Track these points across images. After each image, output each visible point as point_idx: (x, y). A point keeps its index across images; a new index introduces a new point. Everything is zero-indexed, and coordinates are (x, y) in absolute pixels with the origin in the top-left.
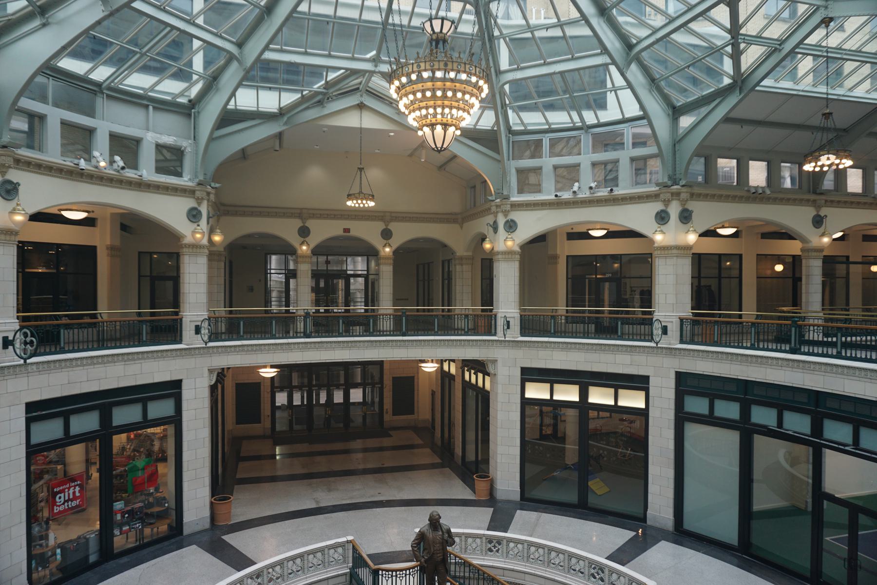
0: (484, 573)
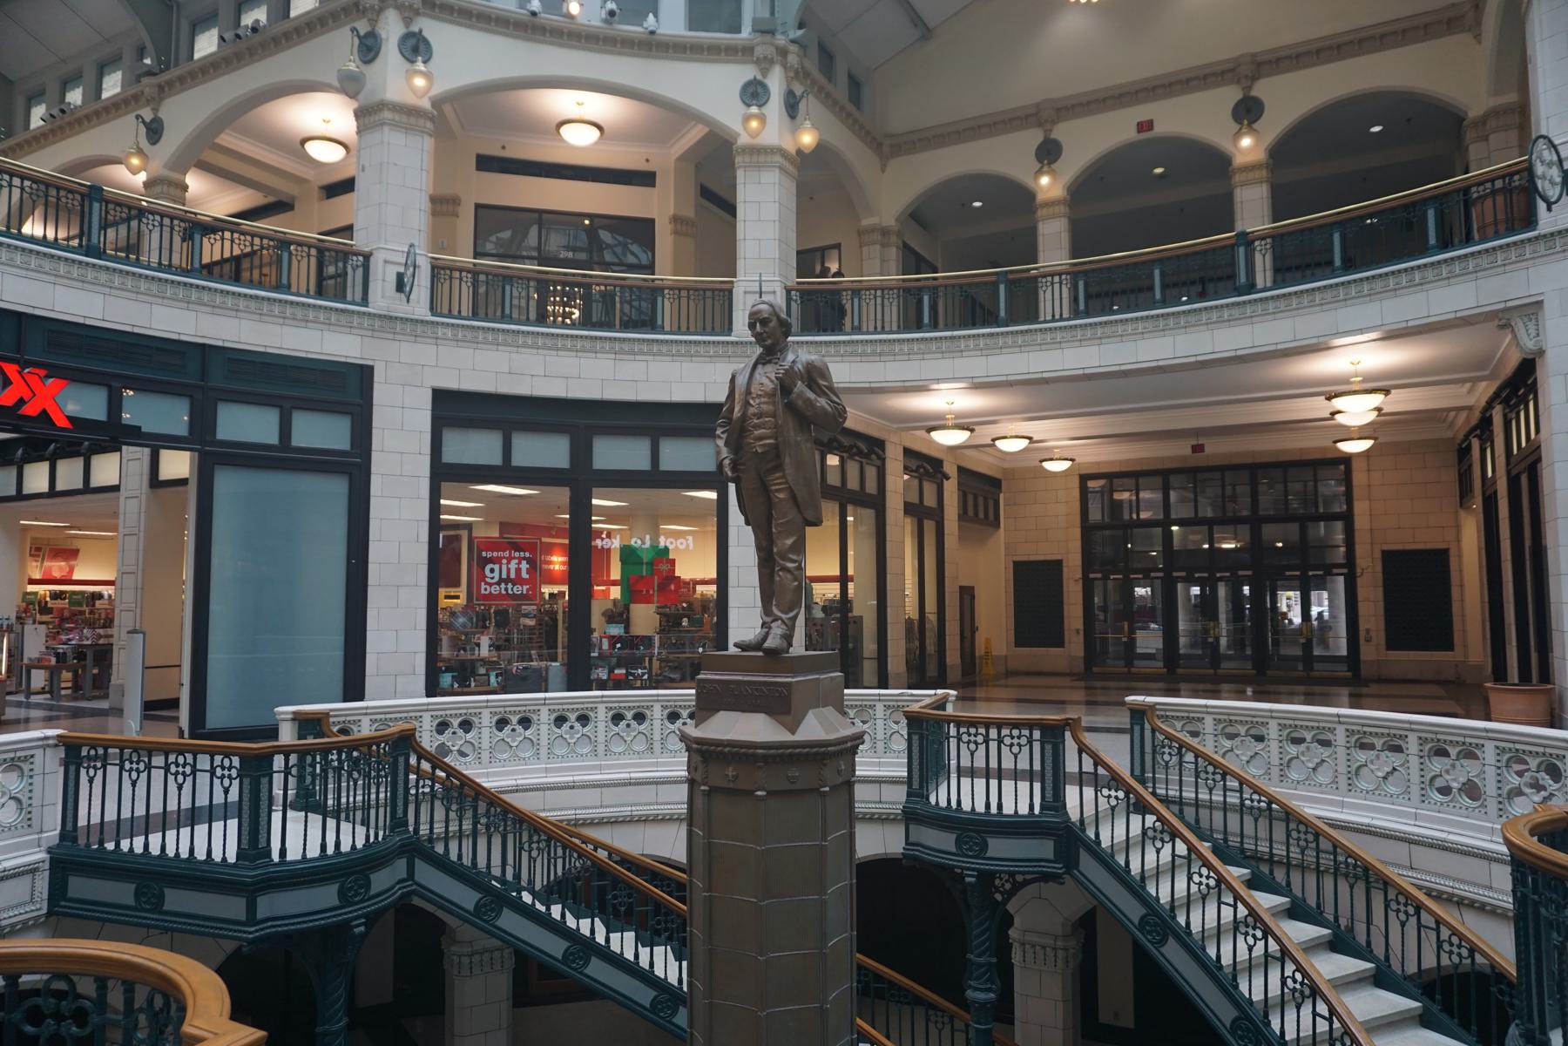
0: (1336, 845)
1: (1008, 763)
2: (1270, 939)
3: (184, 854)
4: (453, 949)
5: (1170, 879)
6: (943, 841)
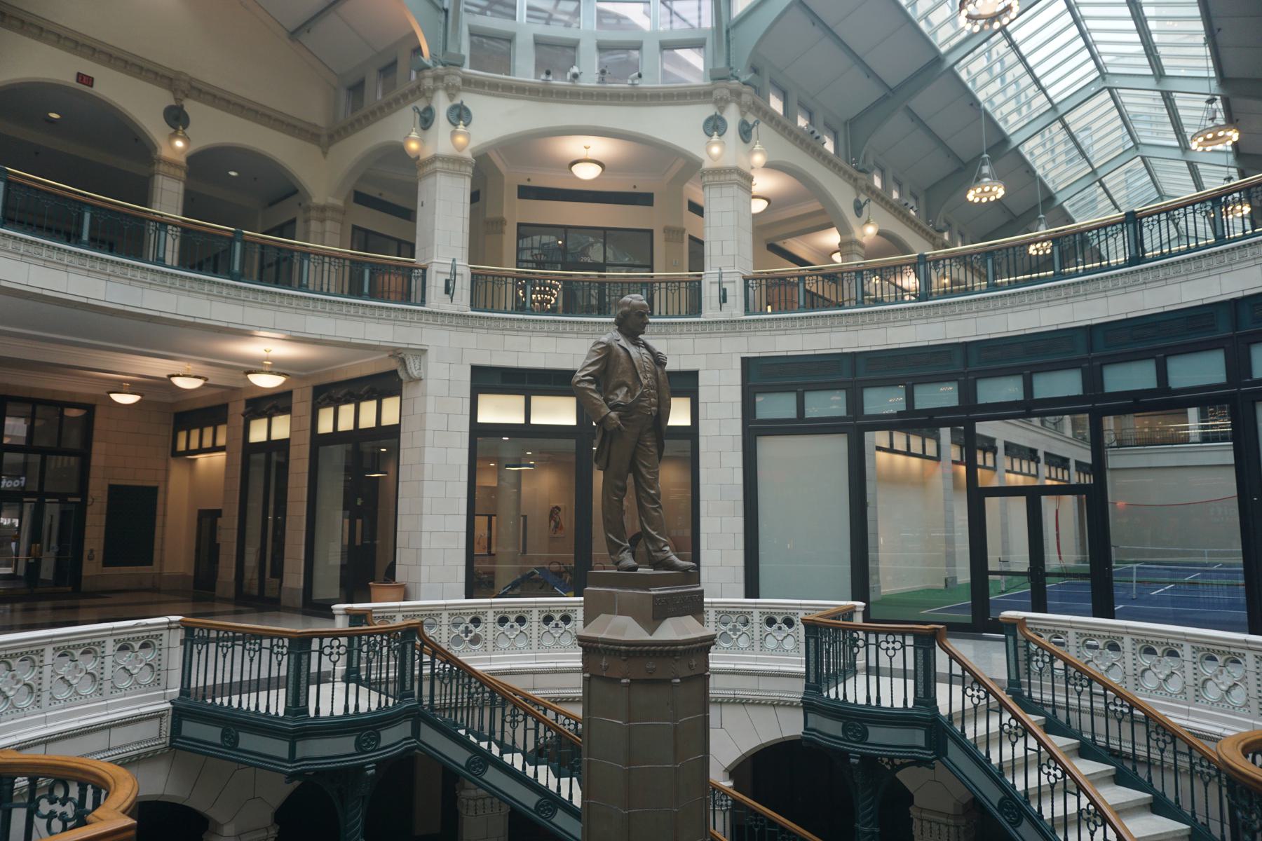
1: (884, 662)
2: (1108, 826)
3: (262, 709)
4: (462, 793)
5: (1024, 773)
6: (833, 727)
